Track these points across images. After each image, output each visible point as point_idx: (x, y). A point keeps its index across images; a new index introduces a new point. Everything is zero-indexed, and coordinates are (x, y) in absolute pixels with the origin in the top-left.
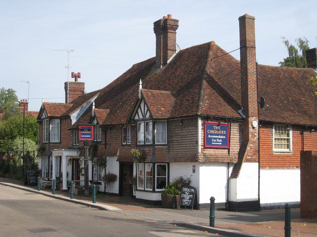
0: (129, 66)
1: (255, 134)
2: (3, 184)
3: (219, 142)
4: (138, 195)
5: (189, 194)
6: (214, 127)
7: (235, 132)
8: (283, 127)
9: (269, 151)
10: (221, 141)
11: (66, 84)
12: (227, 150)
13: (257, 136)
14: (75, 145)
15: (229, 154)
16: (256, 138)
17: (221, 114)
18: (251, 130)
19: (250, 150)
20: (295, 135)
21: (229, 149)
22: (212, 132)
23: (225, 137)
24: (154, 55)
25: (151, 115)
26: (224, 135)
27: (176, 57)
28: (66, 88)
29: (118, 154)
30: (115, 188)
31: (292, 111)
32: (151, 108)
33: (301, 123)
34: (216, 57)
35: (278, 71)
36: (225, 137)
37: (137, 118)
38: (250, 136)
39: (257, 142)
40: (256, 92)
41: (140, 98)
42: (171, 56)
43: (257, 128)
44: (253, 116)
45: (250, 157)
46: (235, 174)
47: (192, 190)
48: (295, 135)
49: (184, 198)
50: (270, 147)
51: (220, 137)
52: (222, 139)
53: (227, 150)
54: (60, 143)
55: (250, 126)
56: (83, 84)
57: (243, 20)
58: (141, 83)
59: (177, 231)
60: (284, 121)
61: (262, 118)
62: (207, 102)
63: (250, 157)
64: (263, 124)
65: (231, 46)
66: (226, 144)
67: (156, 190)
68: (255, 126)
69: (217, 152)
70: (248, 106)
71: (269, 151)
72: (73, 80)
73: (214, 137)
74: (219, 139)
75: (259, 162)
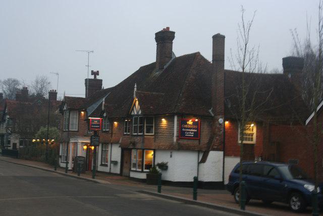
0: (136, 68)
4: (132, 175)
11: (86, 80)
12: (198, 141)
13: (223, 131)
14: (125, 133)
15: (199, 143)
21: (199, 140)
23: (196, 131)
24: (154, 60)
27: (171, 63)
28: (86, 84)
29: (120, 142)
30: (117, 170)
36: (196, 131)
37: (133, 113)
38: (217, 130)
42: (167, 62)
46: (204, 160)
51: (192, 130)
52: (194, 132)
53: (198, 141)
54: (78, 131)
56: (101, 81)
58: (136, 86)
65: (208, 56)
67: (145, 170)
72: (92, 77)
73: (187, 130)
74: (192, 132)
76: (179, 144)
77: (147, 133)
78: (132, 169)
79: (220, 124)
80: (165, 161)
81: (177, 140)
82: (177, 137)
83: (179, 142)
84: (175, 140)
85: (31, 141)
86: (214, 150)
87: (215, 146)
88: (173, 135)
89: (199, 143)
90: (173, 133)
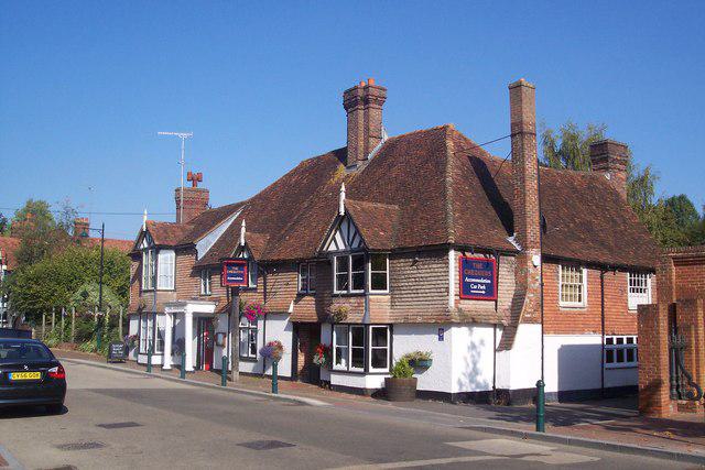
2: (494, 455)
4: (335, 380)
8: (575, 264)
16: (537, 284)
17: (485, 244)
18: (531, 270)
25: (362, 241)
32: (364, 231)
33: (601, 260)
34: (459, 148)
38: (529, 279)
41: (342, 214)
46: (507, 344)
51: (482, 281)
52: (486, 284)
55: (529, 264)
59: (488, 457)
64: (546, 259)
66: (491, 293)
73: (473, 280)
74: (482, 284)
77: (355, 289)
78: (335, 367)
80: (423, 350)
81: (457, 302)
83: (460, 306)
84: (452, 303)
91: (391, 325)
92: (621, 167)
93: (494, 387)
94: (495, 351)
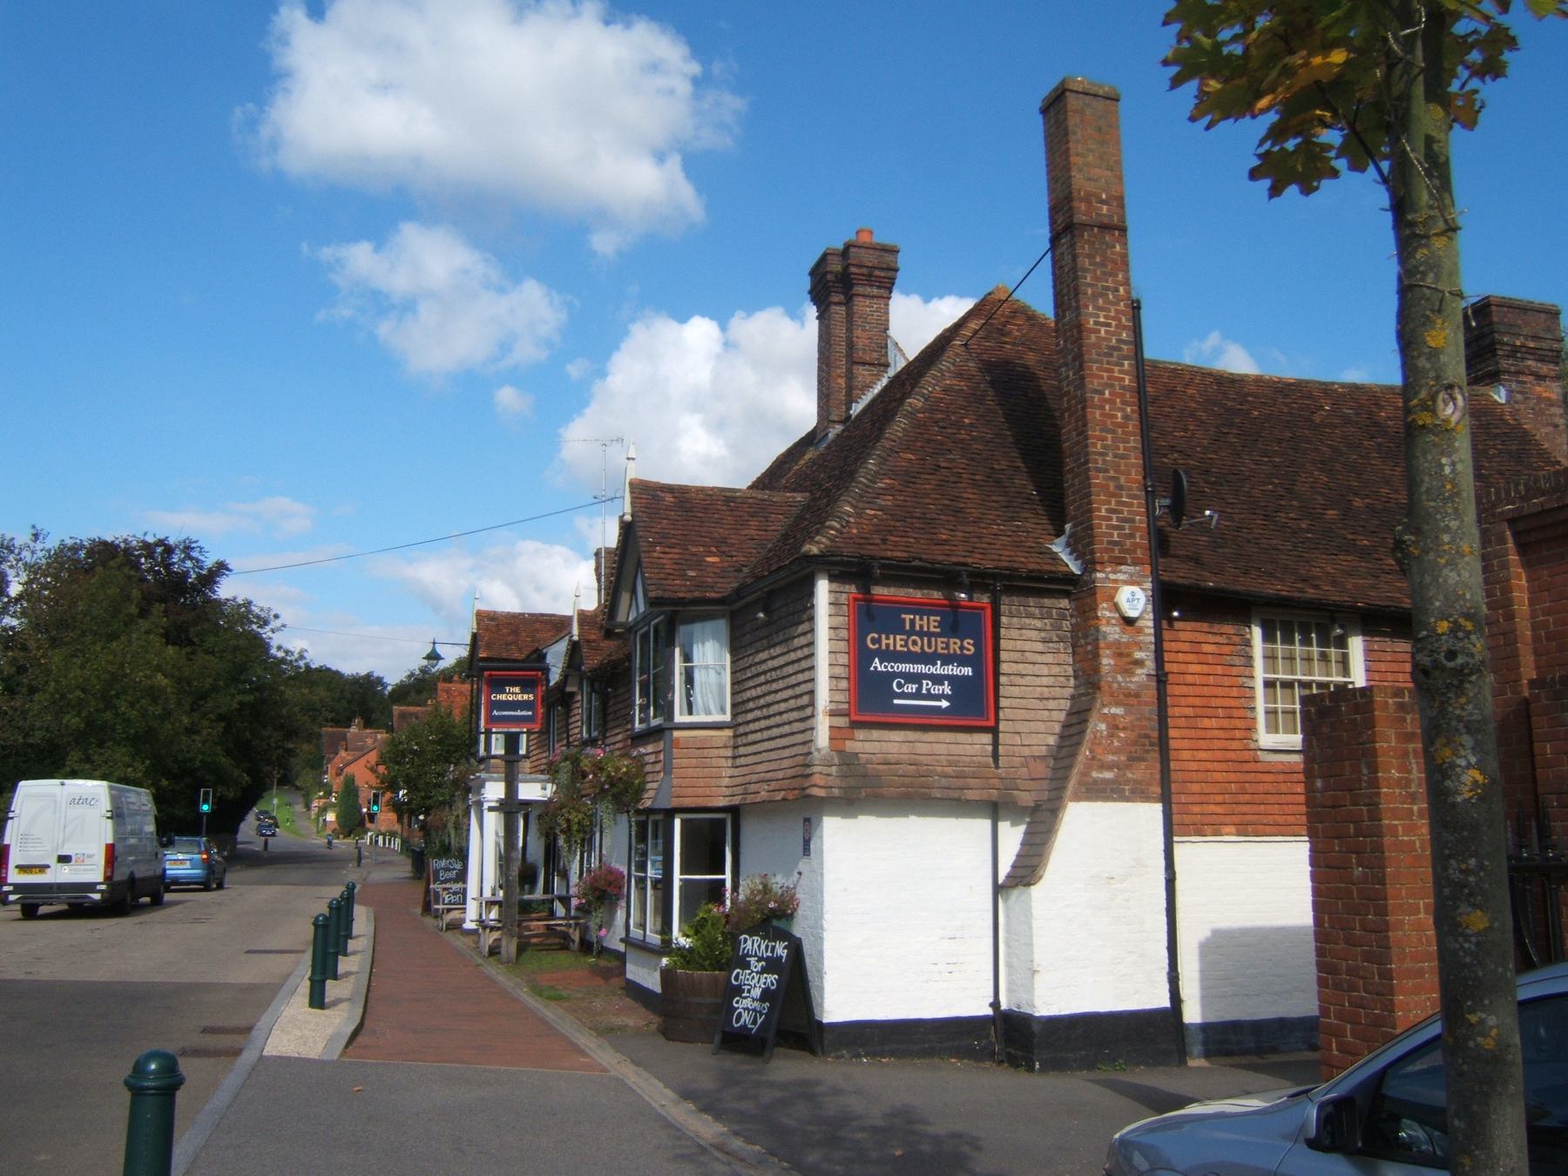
1: (1138, 655)
3: (938, 697)
5: (763, 971)
6: (908, 617)
7: (1028, 646)
9: (1235, 745)
10: (946, 689)
12: (986, 738)
13: (1150, 665)
16: (1142, 675)
18: (1112, 632)
19: (1111, 736)
20: (1383, 667)
21: (994, 731)
22: (897, 642)
23: (967, 671)
26: (962, 660)
31: (1364, 553)
35: (1310, 397)
36: (967, 671)
38: (1107, 661)
39: (1151, 694)
40: (1134, 442)
43: (1148, 623)
44: (1120, 562)
45: (1108, 775)
46: (1027, 871)
47: (781, 950)
48: (1383, 667)
49: (738, 991)
50: (1240, 724)
51: (938, 669)
52: (952, 679)
55: (1104, 611)
57: (1055, 105)
60: (1311, 593)
61: (1182, 574)
62: (886, 501)
63: (1108, 775)
64: (1167, 599)
68: (1133, 614)
69: (922, 748)
70: (1090, 511)
71: (1235, 745)
74: (938, 679)
75: (1166, 799)
76: (848, 761)
79: (1129, 622)
82: (833, 714)
83: (851, 746)
84: (822, 737)
85: (1475, 328)
86: (1096, 792)
87: (1104, 766)
88: (812, 704)
89: (995, 755)
90: (812, 693)
91: (735, 811)
92: (1544, 369)
93: (995, 1004)
94: (998, 889)
